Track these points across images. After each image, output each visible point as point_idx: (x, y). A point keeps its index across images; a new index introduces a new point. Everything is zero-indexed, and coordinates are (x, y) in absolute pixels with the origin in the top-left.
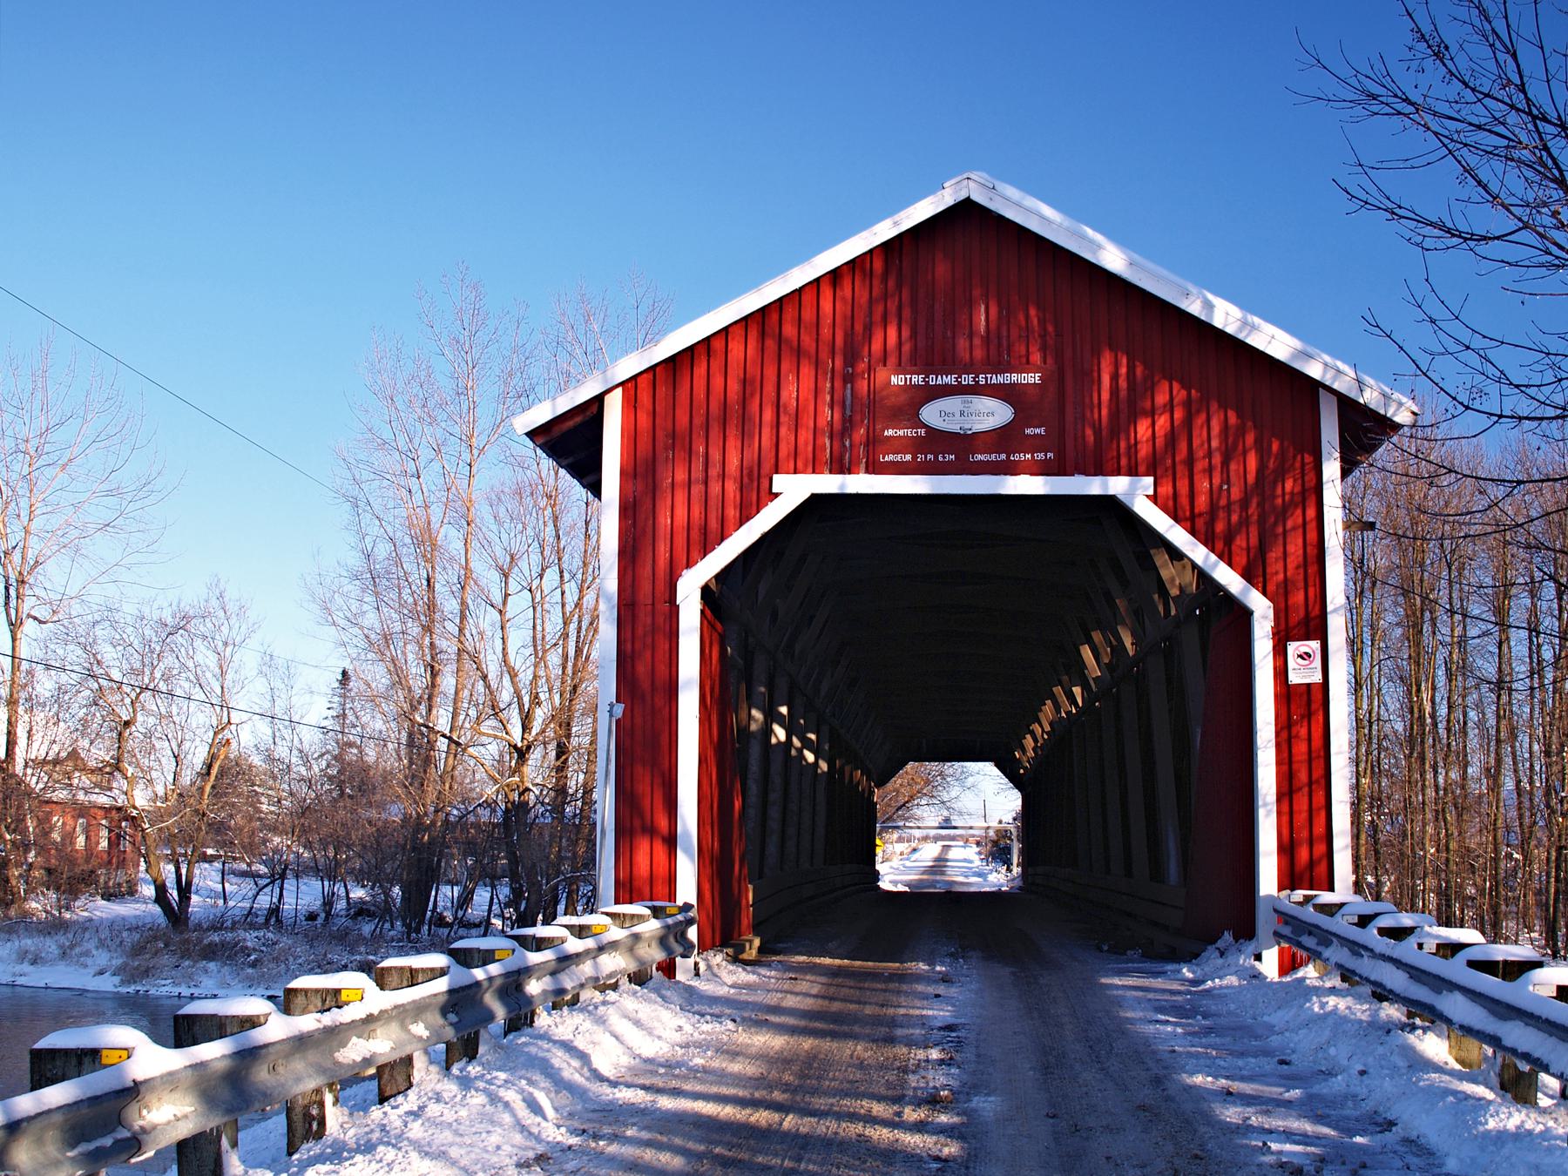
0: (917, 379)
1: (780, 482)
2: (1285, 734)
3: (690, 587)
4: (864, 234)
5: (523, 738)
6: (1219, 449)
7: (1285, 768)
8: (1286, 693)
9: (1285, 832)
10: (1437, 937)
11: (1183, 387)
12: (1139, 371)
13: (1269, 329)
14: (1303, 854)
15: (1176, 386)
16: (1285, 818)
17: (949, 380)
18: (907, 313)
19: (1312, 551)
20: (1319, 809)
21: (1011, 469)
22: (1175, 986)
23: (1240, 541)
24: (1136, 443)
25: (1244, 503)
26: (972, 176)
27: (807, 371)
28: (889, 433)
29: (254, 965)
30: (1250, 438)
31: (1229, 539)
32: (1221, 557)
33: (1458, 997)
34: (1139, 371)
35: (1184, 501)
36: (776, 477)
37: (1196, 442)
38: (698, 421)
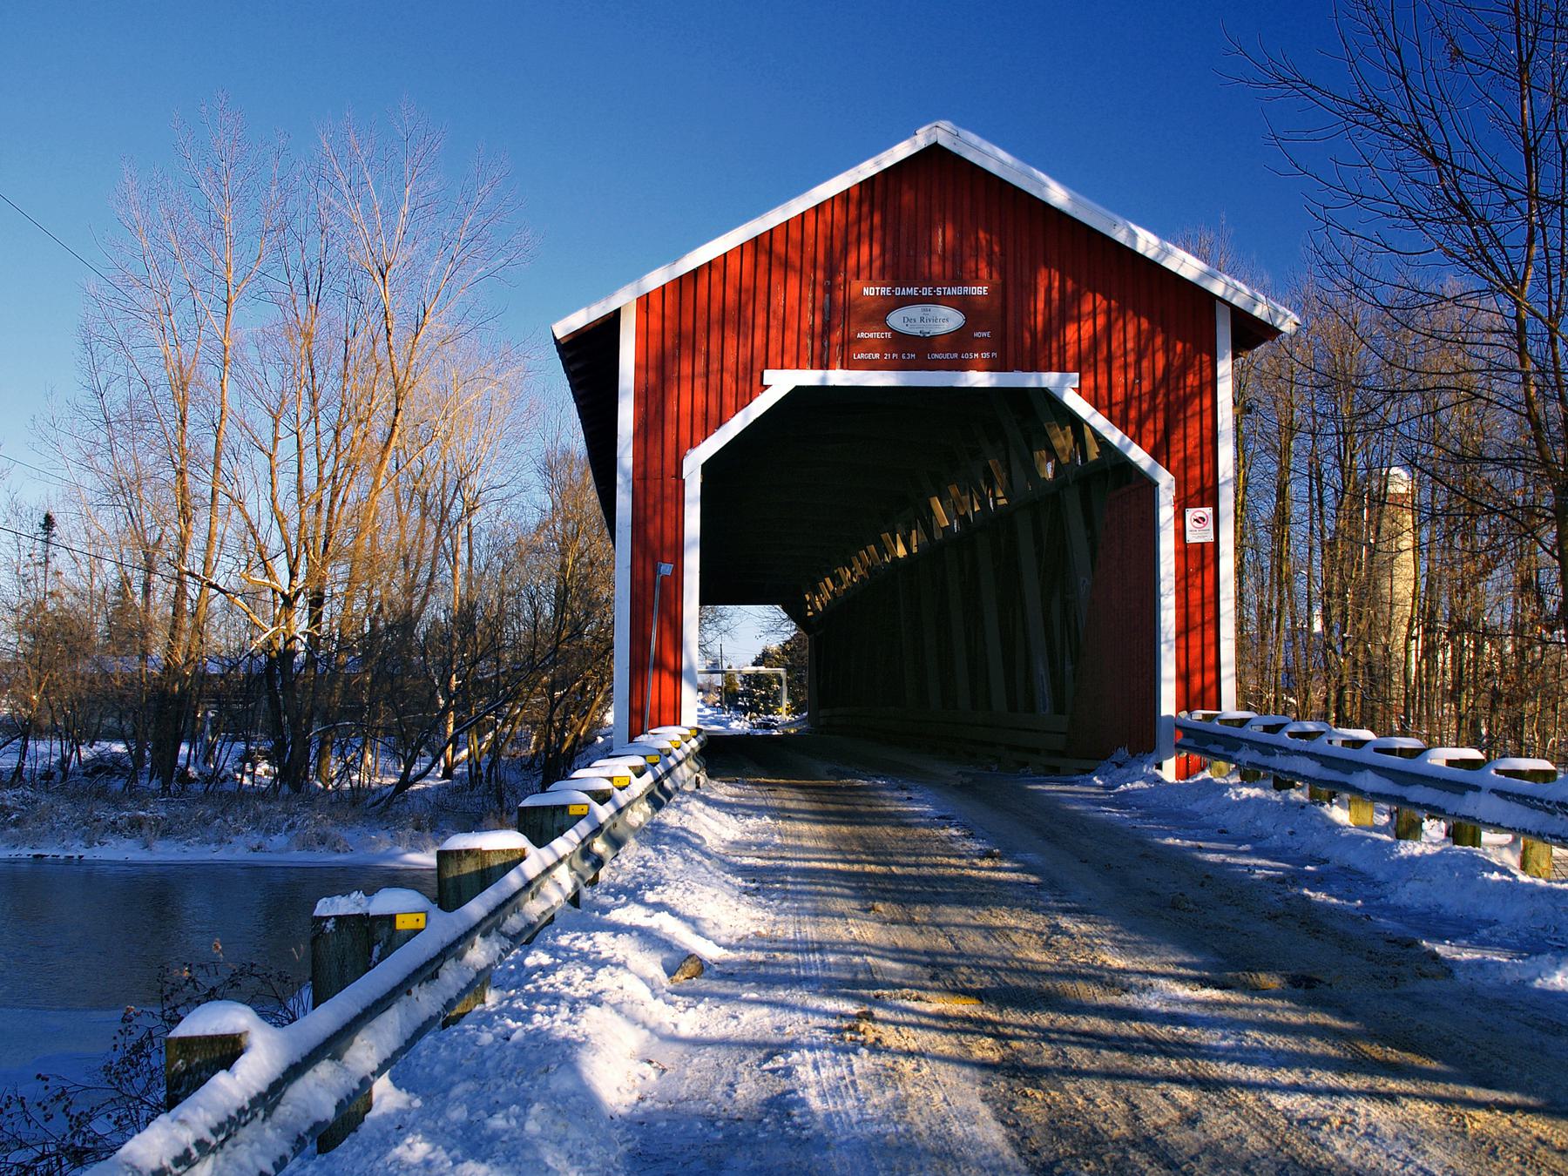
0: (885, 291)
1: (770, 376)
2: (1183, 583)
3: (694, 462)
4: (852, 171)
5: (290, 585)
6: (1133, 350)
7: (1183, 610)
8: (1184, 550)
9: (1183, 663)
10: (1342, 735)
11: (1105, 298)
12: (1069, 284)
13: (1181, 254)
14: (1196, 681)
15: (1098, 297)
16: (1183, 652)
17: (912, 291)
18: (877, 234)
19: (1207, 433)
20: (1210, 645)
21: (963, 366)
22: (1093, 790)
23: (1149, 425)
24: (1065, 345)
25: (1153, 394)
26: (940, 125)
27: (793, 282)
28: (862, 335)
29: (16, 824)
30: (1159, 341)
31: (1140, 424)
32: (1133, 439)
33: (1369, 774)
34: (1069, 284)
35: (1103, 392)
36: (766, 373)
37: (1114, 345)
38: (701, 324)
